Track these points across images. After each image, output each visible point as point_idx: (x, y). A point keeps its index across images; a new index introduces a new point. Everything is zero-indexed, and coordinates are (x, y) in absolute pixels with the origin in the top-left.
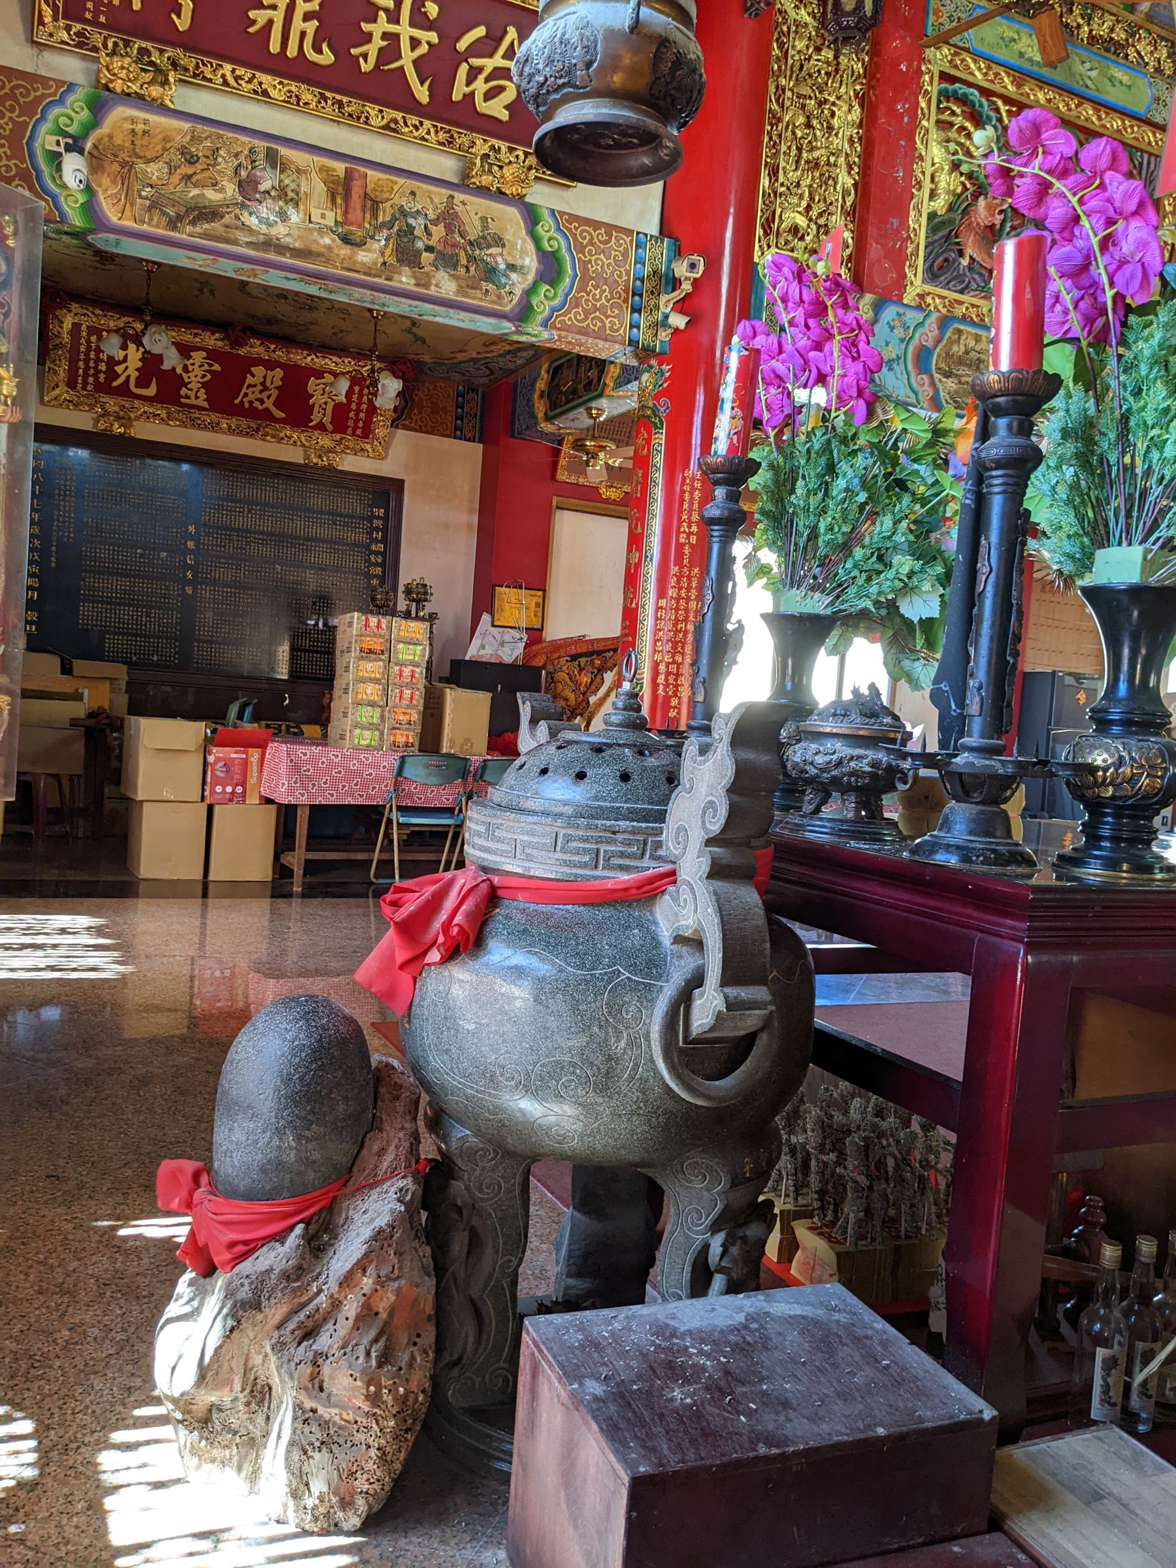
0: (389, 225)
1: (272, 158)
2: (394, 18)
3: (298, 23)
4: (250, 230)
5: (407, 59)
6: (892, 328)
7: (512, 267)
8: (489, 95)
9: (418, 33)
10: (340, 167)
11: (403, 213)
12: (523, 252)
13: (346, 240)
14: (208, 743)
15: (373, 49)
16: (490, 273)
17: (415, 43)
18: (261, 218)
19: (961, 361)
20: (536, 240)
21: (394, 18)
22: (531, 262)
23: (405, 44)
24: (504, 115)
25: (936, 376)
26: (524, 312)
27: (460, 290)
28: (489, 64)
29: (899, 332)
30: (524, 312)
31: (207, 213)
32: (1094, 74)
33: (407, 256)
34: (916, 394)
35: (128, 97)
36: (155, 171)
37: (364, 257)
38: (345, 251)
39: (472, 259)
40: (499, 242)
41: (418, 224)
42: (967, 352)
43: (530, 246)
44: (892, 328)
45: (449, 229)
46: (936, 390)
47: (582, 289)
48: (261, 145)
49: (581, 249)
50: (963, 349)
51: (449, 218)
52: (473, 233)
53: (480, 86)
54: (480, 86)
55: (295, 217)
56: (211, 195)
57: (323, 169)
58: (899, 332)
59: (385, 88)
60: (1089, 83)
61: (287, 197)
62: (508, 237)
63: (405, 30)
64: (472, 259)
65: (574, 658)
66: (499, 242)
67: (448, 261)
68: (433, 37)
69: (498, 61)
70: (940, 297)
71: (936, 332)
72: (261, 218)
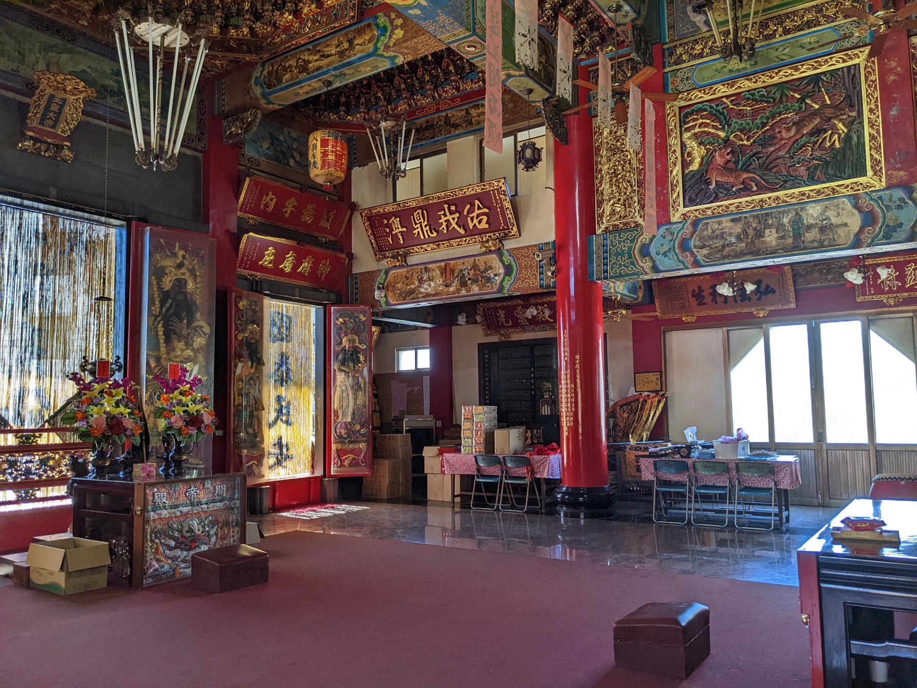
0: (457, 276)
1: (426, 269)
2: (445, 215)
3: (425, 229)
4: (422, 293)
5: (454, 225)
6: (664, 237)
7: (496, 275)
8: (480, 222)
9: (453, 216)
10: (443, 264)
11: (461, 271)
12: (499, 268)
13: (446, 286)
14: (441, 453)
15: (444, 226)
16: (489, 280)
17: (454, 219)
18: (426, 288)
19: (710, 238)
20: (502, 261)
21: (445, 215)
22: (502, 271)
23: (451, 220)
24: (487, 226)
25: (695, 250)
26: (501, 287)
27: (480, 289)
28: (474, 214)
29: (669, 237)
30: (501, 287)
31: (412, 292)
32: (786, 51)
33: (463, 284)
34: (683, 263)
35: (391, 269)
36: (399, 285)
37: (451, 289)
38: (446, 289)
39: (483, 277)
40: (491, 268)
41: (465, 272)
42: (713, 232)
43: (501, 265)
44: (664, 237)
45: (475, 270)
46: (695, 257)
47: (520, 273)
48: (423, 267)
49: (518, 259)
50: (710, 231)
51: (475, 267)
52: (482, 269)
53: (476, 221)
54: (476, 221)
55: (432, 284)
56: (412, 286)
57: (439, 267)
58: (669, 237)
59: (452, 235)
60: (784, 57)
61: (430, 279)
62: (493, 265)
63: (449, 217)
64: (483, 277)
65: (621, 406)
66: (491, 268)
67: (475, 281)
68: (457, 215)
69: (477, 212)
70: (696, 210)
71: (691, 229)
72: (426, 288)
